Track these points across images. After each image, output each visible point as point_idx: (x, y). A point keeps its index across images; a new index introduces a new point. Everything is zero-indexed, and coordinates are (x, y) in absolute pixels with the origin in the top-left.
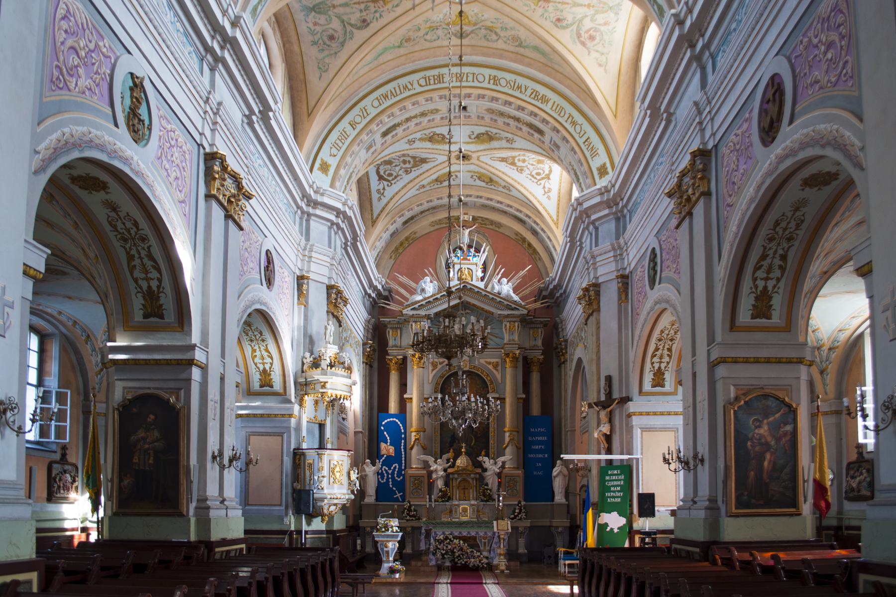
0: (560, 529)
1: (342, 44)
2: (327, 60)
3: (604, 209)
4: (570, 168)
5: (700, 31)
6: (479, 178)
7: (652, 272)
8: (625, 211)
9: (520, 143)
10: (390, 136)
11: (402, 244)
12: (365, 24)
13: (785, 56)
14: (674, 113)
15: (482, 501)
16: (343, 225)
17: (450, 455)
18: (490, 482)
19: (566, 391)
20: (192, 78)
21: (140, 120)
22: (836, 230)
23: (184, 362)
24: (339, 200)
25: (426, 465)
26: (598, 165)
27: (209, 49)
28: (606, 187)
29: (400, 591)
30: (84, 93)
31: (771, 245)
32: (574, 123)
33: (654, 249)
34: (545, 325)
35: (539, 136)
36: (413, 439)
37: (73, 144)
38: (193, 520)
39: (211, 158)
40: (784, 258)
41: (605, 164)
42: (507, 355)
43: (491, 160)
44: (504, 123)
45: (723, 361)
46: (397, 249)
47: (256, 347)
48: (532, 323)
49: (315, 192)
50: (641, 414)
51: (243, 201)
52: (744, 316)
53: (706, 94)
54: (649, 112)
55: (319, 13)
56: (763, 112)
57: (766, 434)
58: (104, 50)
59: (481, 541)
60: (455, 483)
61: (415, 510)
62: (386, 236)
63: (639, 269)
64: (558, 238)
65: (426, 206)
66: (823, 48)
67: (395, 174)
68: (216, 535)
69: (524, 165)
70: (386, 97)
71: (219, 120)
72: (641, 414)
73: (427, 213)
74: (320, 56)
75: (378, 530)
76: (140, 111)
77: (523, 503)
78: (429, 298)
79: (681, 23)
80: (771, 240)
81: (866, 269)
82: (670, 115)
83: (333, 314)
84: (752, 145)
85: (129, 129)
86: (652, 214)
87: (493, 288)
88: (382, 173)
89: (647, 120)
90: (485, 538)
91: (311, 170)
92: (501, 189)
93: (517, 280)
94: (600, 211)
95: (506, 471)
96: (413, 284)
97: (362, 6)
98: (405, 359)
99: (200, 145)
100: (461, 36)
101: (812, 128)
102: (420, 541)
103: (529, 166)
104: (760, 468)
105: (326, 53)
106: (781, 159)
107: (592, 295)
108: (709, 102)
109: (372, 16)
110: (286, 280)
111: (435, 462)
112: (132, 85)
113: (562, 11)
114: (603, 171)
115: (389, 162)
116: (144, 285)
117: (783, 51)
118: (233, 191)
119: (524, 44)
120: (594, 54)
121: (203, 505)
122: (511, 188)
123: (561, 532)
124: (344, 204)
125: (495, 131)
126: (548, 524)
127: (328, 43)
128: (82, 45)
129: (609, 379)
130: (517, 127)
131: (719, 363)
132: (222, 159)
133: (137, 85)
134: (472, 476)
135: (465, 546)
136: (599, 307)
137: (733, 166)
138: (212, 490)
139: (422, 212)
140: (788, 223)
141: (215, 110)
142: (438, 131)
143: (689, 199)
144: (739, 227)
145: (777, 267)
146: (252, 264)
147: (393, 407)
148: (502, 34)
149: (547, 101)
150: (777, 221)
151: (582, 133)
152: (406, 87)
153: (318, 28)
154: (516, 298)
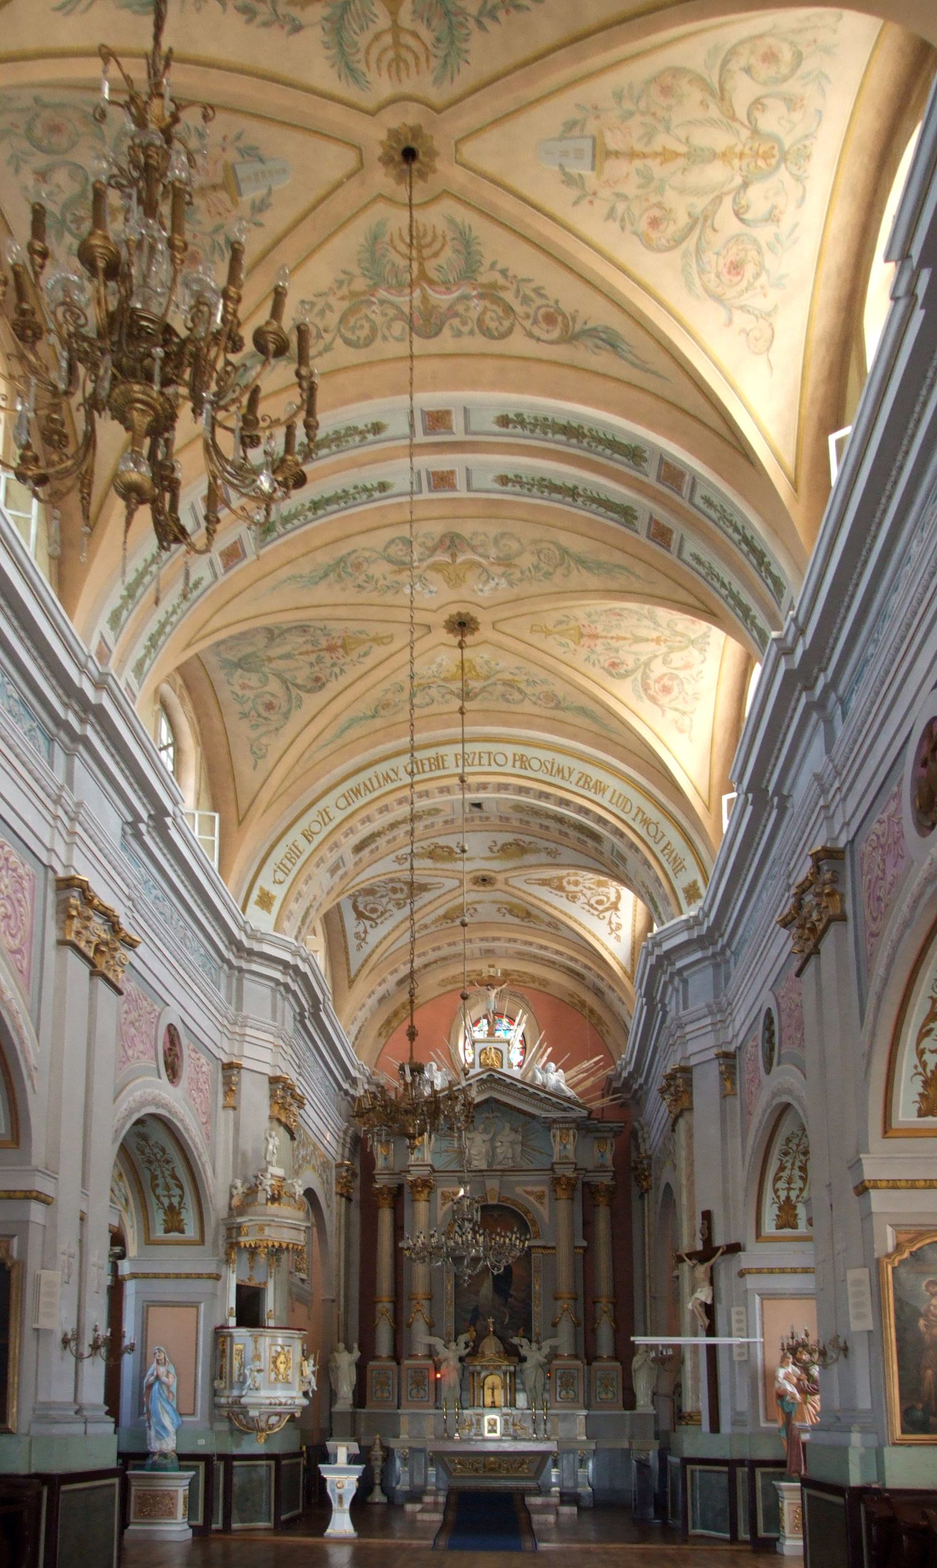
1: (286, 716)
2: (264, 741)
3: (695, 951)
4: (643, 890)
6: (510, 912)
9: (567, 855)
10: (366, 851)
12: (318, 684)
14: (789, 796)
16: (294, 986)
23: (18, 1194)
26: (685, 884)
28: (695, 918)
33: (769, 1009)
34: (617, 1134)
35: (595, 845)
39: (67, 884)
41: (695, 882)
42: (556, 1182)
44: (541, 826)
46: (388, 1022)
47: (158, 1172)
49: (248, 936)
50: (759, 1271)
51: (123, 950)
53: (832, 760)
54: (750, 796)
55: (249, 670)
63: (751, 1043)
67: (381, 909)
69: (577, 889)
70: (357, 792)
71: (78, 829)
72: (759, 1271)
73: (434, 966)
74: (253, 735)
79: (789, 652)
82: (784, 799)
83: (279, 1120)
87: (534, 1077)
88: (361, 908)
89: (750, 809)
92: (544, 927)
94: (688, 954)
97: (313, 658)
99: (48, 867)
103: (585, 891)
105: (263, 729)
107: (680, 1084)
108: (838, 774)
109: (328, 671)
110: (204, 1069)
113: (617, 651)
114: (692, 893)
115: (370, 892)
118: (104, 936)
119: (563, 705)
120: (671, 715)
122: (561, 926)
125: (527, 839)
127: (264, 714)
129: (707, 1216)
132: (84, 889)
136: (691, 1103)
137: (877, 872)
139: (426, 966)
142: (442, 841)
143: (813, 929)
148: (529, 690)
151: (660, 835)
152: (387, 778)
153: (249, 694)
154: (570, 1093)
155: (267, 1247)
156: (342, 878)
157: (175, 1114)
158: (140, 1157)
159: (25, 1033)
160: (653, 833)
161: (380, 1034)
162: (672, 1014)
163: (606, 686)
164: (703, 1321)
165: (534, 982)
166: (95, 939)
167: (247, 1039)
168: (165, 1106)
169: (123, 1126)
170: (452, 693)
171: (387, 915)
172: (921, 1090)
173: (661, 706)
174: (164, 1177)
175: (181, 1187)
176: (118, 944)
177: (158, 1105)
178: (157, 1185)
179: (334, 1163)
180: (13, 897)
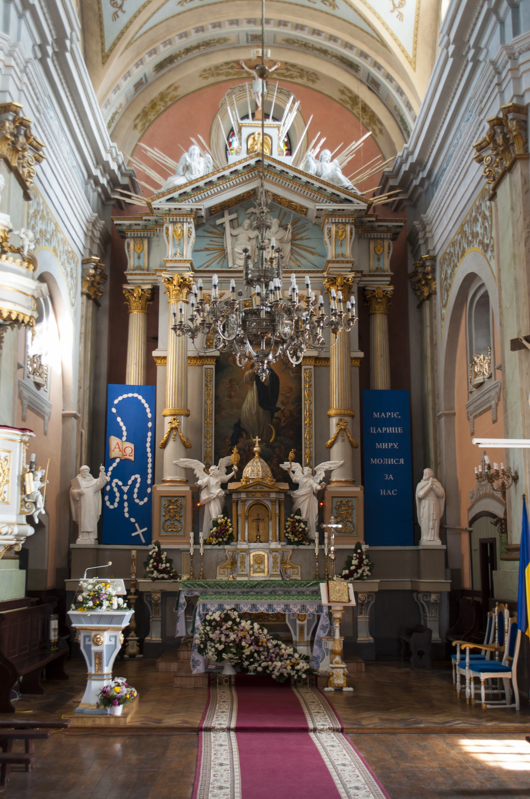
0: (433, 597)
11: (153, 105)
15: (289, 542)
17: (233, 458)
18: (304, 508)
19: (434, 345)
25: (190, 476)
29: (125, 747)
36: (167, 428)
46: (145, 114)
48: (373, 229)
59: (294, 622)
60: (241, 510)
61: (168, 560)
62: (127, 85)
65: (194, 38)
73: (196, 52)
75: (79, 605)
77: (364, 547)
78: (197, 180)
87: (307, 166)
89: (451, 61)
90: (301, 618)
93: (346, 156)
95: (332, 488)
96: (170, 162)
98: (155, 290)
102: (176, 619)
111: (206, 470)
123: (435, 603)
126: (408, 587)
134: (273, 495)
135: (264, 635)
139: (188, 50)
147: (134, 374)
154: (346, 182)
161: (135, 126)
165: (301, 77)
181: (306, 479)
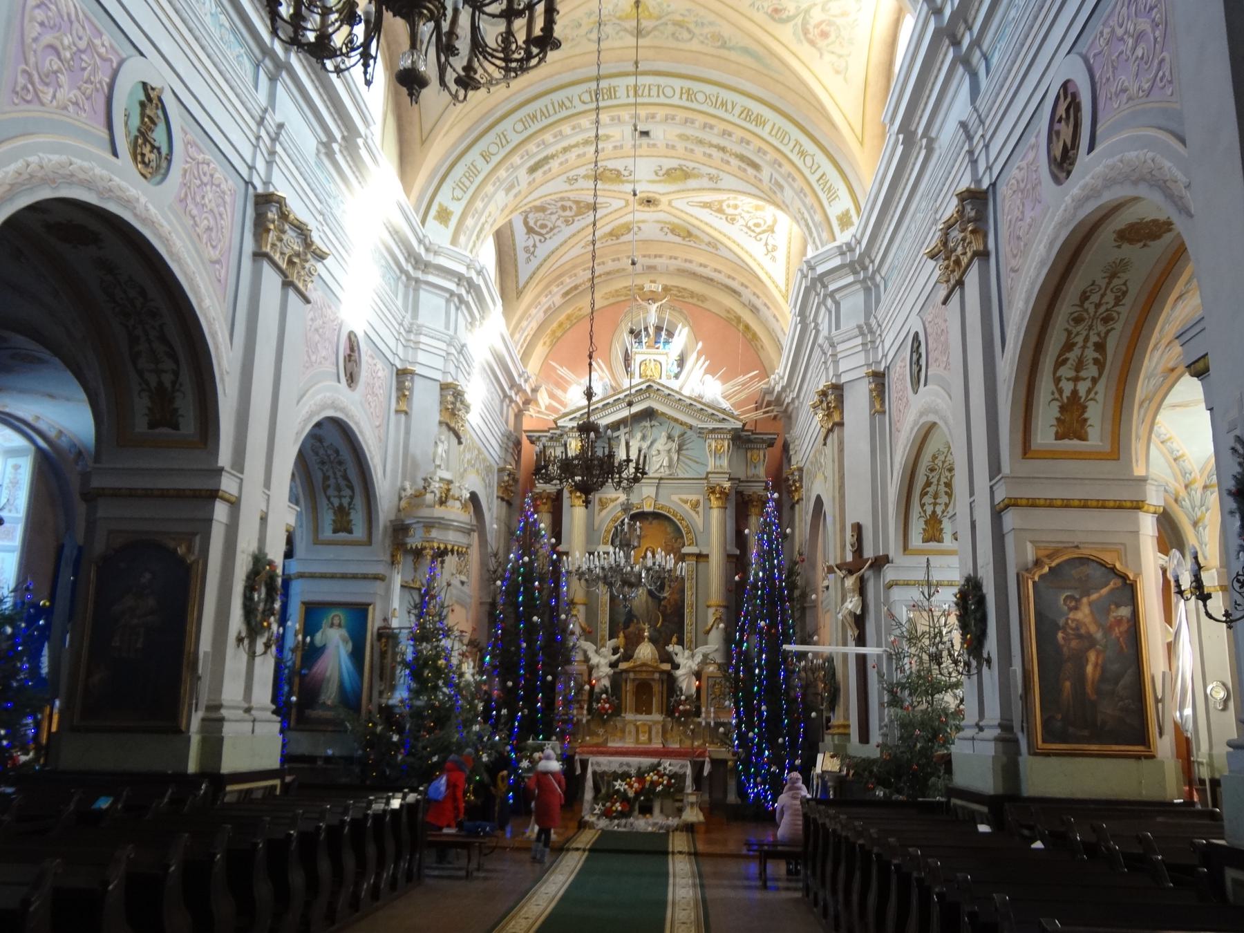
5: (966, 21)
6: (672, 231)
7: (915, 368)
8: (878, 278)
9: (728, 181)
10: (539, 173)
13: (1080, 54)
20: (239, 91)
21: (153, 147)
22: (1180, 305)
24: (460, 261)
27: (267, 52)
30: (65, 108)
31: (1079, 328)
32: (802, 154)
33: (917, 334)
37: (42, 179)
38: (195, 739)
39: (265, 201)
40: (1100, 347)
41: (848, 211)
42: (712, 490)
43: (686, 205)
44: (705, 154)
45: (1012, 503)
47: (330, 473)
51: (312, 262)
52: (1044, 436)
53: (976, 110)
54: (901, 137)
56: (1052, 134)
57: (1088, 620)
58: (102, 50)
63: (899, 363)
64: (786, 320)
66: (1131, 41)
67: (550, 225)
68: (231, 763)
69: (736, 212)
70: (533, 118)
76: (154, 135)
80: (1078, 321)
81: (1201, 365)
82: (931, 142)
83: (448, 425)
84: (1040, 183)
85: (135, 159)
86: (913, 279)
88: (531, 224)
89: (900, 148)
91: (423, 222)
92: (703, 246)
94: (840, 277)
99: (248, 183)
100: (639, 33)
101: (1119, 157)
103: (744, 214)
104: (1080, 678)
106: (1080, 202)
107: (833, 398)
110: (380, 374)
112: (143, 98)
114: (845, 221)
115: (542, 209)
116: (153, 380)
117: (1075, 50)
118: (296, 248)
121: (214, 715)
122: (719, 245)
124: (468, 267)
125: (691, 165)
128: (66, 42)
129: (858, 528)
130: (722, 160)
131: (1007, 507)
132: (281, 202)
133: (150, 100)
137: (1017, 213)
138: (232, 692)
140: (1103, 296)
141: (273, 135)
144: (1027, 302)
145: (1091, 361)
146: (325, 351)
148: (697, 31)
149: (764, 123)
150: (1084, 292)
152: (562, 105)
154: (726, 405)
155: (432, 548)
156: (516, 196)
157: (352, 417)
158: (314, 458)
159: (220, 339)
160: (809, 163)
162: (824, 332)
163: (770, 30)
164: (852, 633)
166: (288, 252)
167: (421, 346)
168: (342, 410)
169: (303, 429)
170: (625, 30)
171: (556, 231)
172: (1058, 415)
173: (819, 50)
174: (336, 478)
175: (351, 488)
176: (309, 256)
177: (336, 409)
178: (329, 486)
179: (496, 468)
180: (216, 210)
181: (687, 662)
